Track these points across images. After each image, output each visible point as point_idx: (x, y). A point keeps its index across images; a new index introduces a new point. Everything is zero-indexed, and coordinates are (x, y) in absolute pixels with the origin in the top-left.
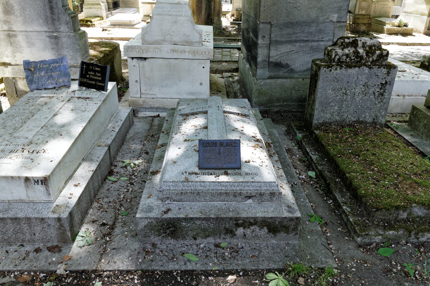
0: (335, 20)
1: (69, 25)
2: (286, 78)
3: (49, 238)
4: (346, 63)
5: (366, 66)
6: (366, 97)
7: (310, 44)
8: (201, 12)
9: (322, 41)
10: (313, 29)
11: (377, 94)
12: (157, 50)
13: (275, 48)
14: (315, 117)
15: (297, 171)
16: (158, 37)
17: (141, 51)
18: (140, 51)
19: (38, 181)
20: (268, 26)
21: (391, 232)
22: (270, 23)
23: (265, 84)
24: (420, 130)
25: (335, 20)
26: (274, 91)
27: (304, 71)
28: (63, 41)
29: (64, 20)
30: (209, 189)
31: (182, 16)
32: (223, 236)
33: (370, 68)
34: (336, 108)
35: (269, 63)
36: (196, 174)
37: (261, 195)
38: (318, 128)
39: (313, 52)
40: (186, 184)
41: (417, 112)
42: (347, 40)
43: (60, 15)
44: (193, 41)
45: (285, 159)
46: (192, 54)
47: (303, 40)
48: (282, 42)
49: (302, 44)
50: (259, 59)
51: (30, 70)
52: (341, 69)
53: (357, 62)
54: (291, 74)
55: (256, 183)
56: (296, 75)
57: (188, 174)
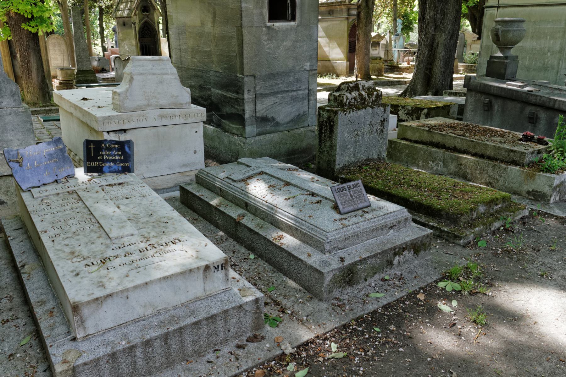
0: (308, 69)
1: (16, 98)
2: (273, 132)
3: (244, 329)
4: (355, 105)
5: (369, 106)
6: (372, 136)
7: (291, 94)
8: (29, 74)
9: (300, 90)
10: (291, 79)
11: (379, 131)
12: (141, 118)
13: (260, 102)
14: (337, 162)
16: (141, 102)
17: (121, 122)
18: (120, 122)
19: (218, 266)
20: (252, 79)
21: (477, 229)
22: (253, 76)
23: (256, 142)
24: (402, 160)
25: (308, 69)
26: (264, 147)
27: (288, 123)
28: (7, 121)
29: (8, 91)
31: (167, 74)
32: (385, 269)
33: (373, 108)
34: (352, 150)
35: (257, 118)
37: (399, 222)
38: (341, 173)
39: (294, 102)
40: (346, 229)
41: (396, 145)
42: (351, 85)
43: (2, 85)
44: (182, 102)
46: (183, 118)
47: (284, 91)
48: (266, 94)
49: (284, 95)
50: (247, 116)
51: (17, 161)
52: (353, 111)
53: (362, 104)
54: (277, 128)
56: (281, 128)
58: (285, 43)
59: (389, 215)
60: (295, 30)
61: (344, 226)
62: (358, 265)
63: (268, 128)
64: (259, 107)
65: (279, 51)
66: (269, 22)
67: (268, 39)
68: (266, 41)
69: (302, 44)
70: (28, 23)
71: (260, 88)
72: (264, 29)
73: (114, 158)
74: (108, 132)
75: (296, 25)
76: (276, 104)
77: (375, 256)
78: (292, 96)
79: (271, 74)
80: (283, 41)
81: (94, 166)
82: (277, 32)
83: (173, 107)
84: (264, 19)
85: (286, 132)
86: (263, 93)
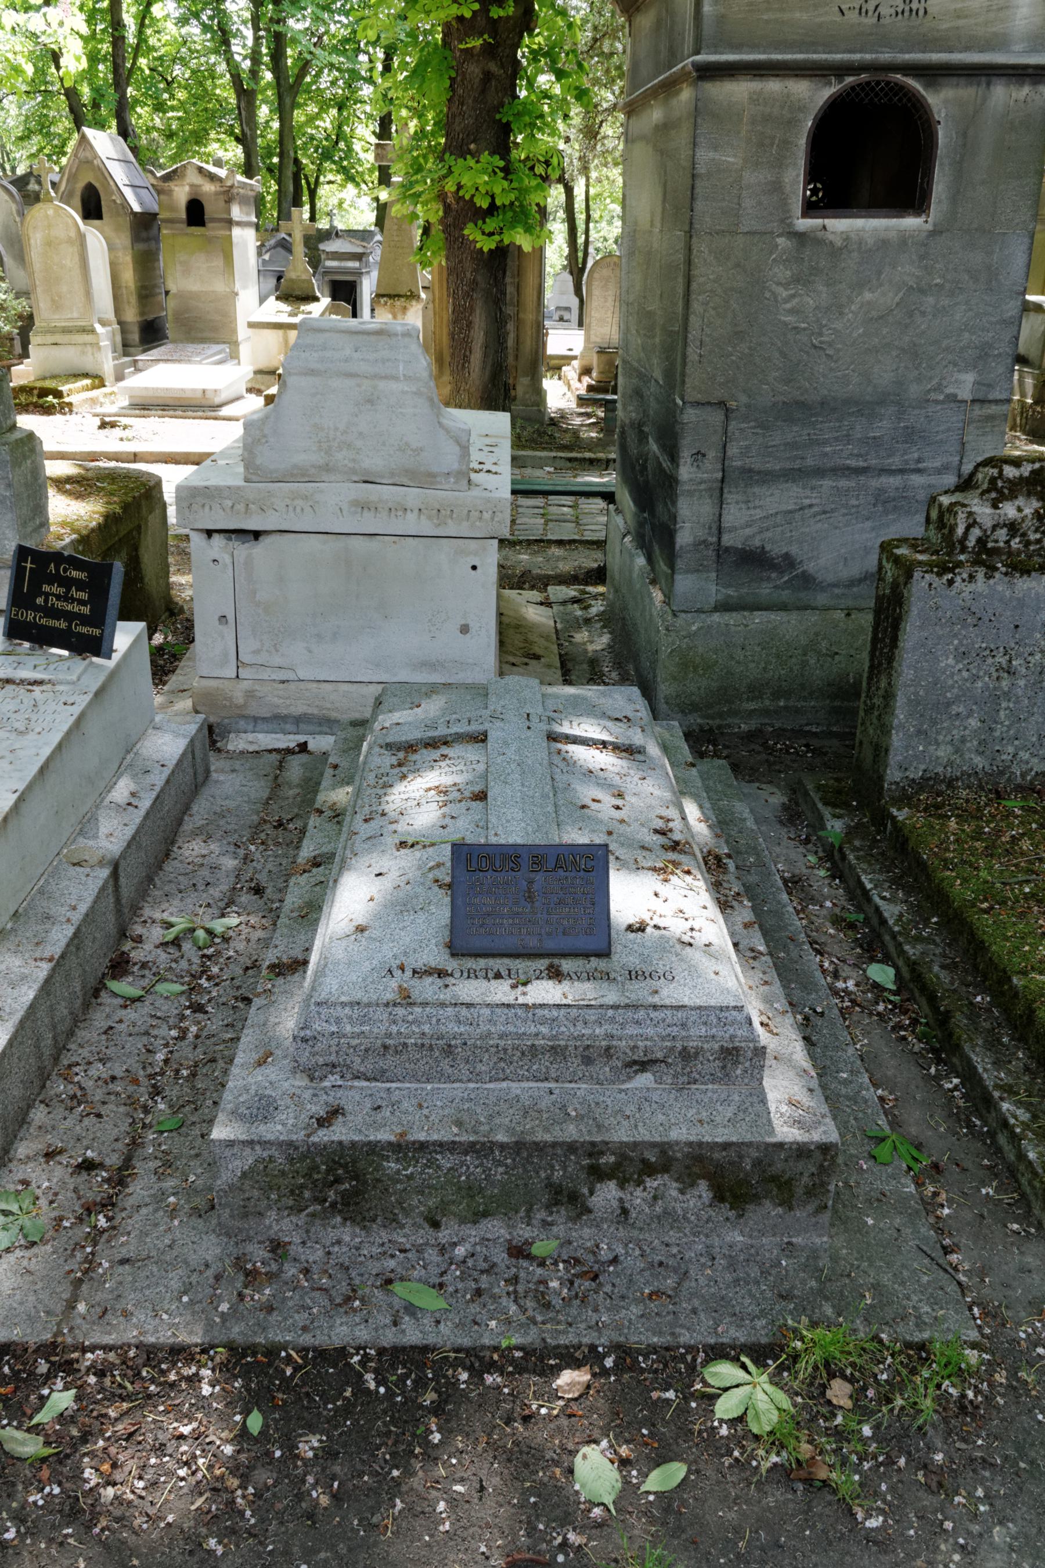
2: (783, 607)
7: (875, 483)
9: (919, 471)
10: (883, 427)
12: (299, 502)
13: (739, 497)
14: (895, 758)
15: (826, 964)
18: (237, 507)
20: (716, 417)
26: (739, 655)
30: (489, 1034)
31: (395, 378)
32: (541, 1215)
34: (974, 723)
35: (721, 553)
36: (441, 973)
38: (904, 799)
39: (886, 512)
40: (400, 1011)
42: (1010, 472)
44: (435, 469)
45: (778, 914)
46: (429, 518)
47: (848, 468)
48: (768, 473)
49: (843, 483)
50: (684, 538)
52: (988, 577)
55: (669, 1012)
56: (822, 599)
57: (409, 973)
58: (868, 296)
59: (641, 1014)
60: (921, 248)
61: (406, 998)
62: (387, 1159)
63: (765, 591)
64: (734, 514)
65: (838, 325)
66: (804, 215)
67: (797, 280)
68: (786, 286)
69: (945, 302)
70: (480, 222)
71: (746, 451)
72: (781, 241)
73: (69, 608)
74: (209, 533)
75: (929, 227)
76: (808, 512)
77: (480, 1149)
78: (881, 490)
79: (797, 403)
80: (860, 285)
81: (25, 621)
82: (836, 252)
83: (406, 481)
84: (784, 204)
85: (839, 615)
86: (757, 466)
